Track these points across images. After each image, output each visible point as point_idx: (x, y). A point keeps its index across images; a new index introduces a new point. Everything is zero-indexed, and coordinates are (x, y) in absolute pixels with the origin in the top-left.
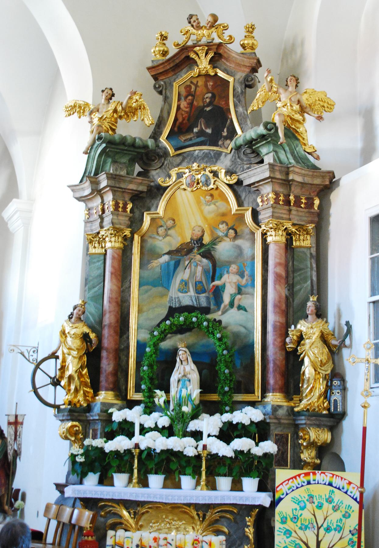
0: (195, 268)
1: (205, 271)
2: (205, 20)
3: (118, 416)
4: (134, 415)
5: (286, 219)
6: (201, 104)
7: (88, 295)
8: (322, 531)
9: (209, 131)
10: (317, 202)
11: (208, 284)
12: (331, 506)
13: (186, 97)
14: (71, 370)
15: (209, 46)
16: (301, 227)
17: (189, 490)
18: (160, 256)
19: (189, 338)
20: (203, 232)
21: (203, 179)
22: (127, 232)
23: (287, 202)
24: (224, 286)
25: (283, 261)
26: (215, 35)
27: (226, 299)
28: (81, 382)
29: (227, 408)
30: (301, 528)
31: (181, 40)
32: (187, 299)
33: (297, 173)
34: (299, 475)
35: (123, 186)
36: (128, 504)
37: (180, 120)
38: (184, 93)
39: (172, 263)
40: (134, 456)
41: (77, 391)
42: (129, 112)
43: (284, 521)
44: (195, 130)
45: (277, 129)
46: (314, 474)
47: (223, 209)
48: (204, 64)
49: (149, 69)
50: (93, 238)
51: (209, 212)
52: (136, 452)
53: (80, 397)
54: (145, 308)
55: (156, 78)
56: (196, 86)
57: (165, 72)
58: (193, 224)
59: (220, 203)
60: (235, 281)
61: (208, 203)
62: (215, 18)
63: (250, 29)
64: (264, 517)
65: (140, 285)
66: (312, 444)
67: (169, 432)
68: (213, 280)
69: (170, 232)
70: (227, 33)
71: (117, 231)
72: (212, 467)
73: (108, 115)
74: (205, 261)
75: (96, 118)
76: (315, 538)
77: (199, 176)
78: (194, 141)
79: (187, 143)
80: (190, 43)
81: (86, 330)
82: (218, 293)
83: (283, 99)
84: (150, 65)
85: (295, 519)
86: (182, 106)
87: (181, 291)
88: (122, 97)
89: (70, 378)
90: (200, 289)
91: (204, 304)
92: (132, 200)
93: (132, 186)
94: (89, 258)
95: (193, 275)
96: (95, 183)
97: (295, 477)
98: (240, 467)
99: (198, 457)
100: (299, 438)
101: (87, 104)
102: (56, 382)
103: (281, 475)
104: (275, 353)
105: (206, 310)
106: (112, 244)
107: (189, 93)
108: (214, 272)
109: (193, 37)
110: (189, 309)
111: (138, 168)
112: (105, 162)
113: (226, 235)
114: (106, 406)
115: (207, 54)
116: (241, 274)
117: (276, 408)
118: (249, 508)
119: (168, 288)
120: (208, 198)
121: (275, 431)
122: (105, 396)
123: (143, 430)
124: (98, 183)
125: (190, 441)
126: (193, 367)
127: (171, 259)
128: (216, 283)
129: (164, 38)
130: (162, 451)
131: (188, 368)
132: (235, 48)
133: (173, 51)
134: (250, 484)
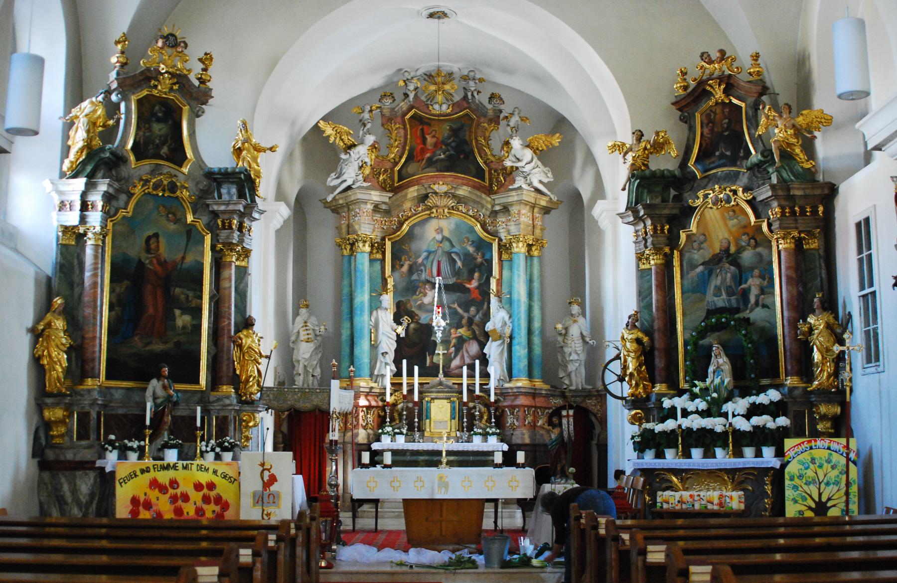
0: (725, 275)
1: (734, 277)
2: (715, 55)
3: (667, 403)
4: (680, 402)
5: (792, 228)
6: (720, 130)
7: (642, 305)
8: (823, 486)
9: (728, 153)
10: (821, 209)
11: (737, 288)
12: (830, 465)
13: (707, 125)
14: (631, 367)
15: (721, 79)
16: (810, 234)
17: (722, 458)
18: (696, 266)
19: (725, 335)
20: (729, 243)
21: (725, 197)
22: (667, 250)
23: (793, 213)
24: (749, 289)
25: (793, 264)
26: (725, 68)
27: (752, 299)
28: (640, 378)
29: (754, 392)
30: (806, 484)
31: (697, 73)
32: (721, 301)
33: (798, 189)
34: (803, 443)
35: (657, 212)
36: (676, 472)
37: (704, 146)
38: (705, 121)
39: (706, 272)
40: (678, 435)
41: (637, 385)
42: (658, 147)
43: (792, 479)
44: (717, 154)
45: (773, 154)
46: (815, 441)
47: (744, 222)
48: (719, 94)
49: (673, 104)
50: (640, 257)
51: (733, 226)
52: (679, 431)
53: (641, 390)
54: (688, 312)
55: (680, 110)
56: (715, 113)
57: (686, 106)
58: (721, 237)
59: (741, 217)
60: (758, 283)
61: (731, 218)
62: (722, 52)
63: (756, 57)
64: (778, 476)
65: (683, 293)
66: (824, 417)
67: (704, 414)
68: (740, 285)
69: (702, 246)
70: (735, 64)
71: (657, 250)
72: (738, 441)
73: (640, 153)
74: (732, 268)
75: (630, 157)
76: (817, 491)
77: (722, 196)
78: (716, 164)
79: (712, 166)
80: (704, 78)
81: (640, 335)
82: (745, 294)
83: (780, 126)
84: (674, 100)
85: (801, 477)
86: (705, 133)
87: (715, 295)
88: (649, 136)
89: (631, 375)
90: (730, 293)
91: (735, 305)
92: (668, 223)
93: (666, 212)
94: (642, 274)
95: (724, 280)
96: (635, 212)
97: (800, 444)
98: (759, 438)
99: (725, 434)
100: (814, 413)
101: (624, 144)
102: (621, 379)
103: (789, 443)
104: (791, 343)
105: (738, 310)
106: (654, 261)
107: (710, 121)
108: (740, 278)
109: (707, 72)
110: (721, 311)
111: (673, 193)
112: (642, 193)
113: (749, 245)
114: (660, 396)
115: (720, 85)
116: (762, 277)
117: (792, 389)
118: (766, 471)
119: (704, 294)
120: (731, 213)
121: (792, 408)
122: (659, 388)
123: (685, 413)
124: (638, 212)
125: (722, 420)
126: (726, 359)
127: (706, 269)
128: (743, 286)
129: (684, 74)
130: (698, 429)
131: (721, 361)
132: (743, 77)
133: (693, 84)
134: (768, 452)
